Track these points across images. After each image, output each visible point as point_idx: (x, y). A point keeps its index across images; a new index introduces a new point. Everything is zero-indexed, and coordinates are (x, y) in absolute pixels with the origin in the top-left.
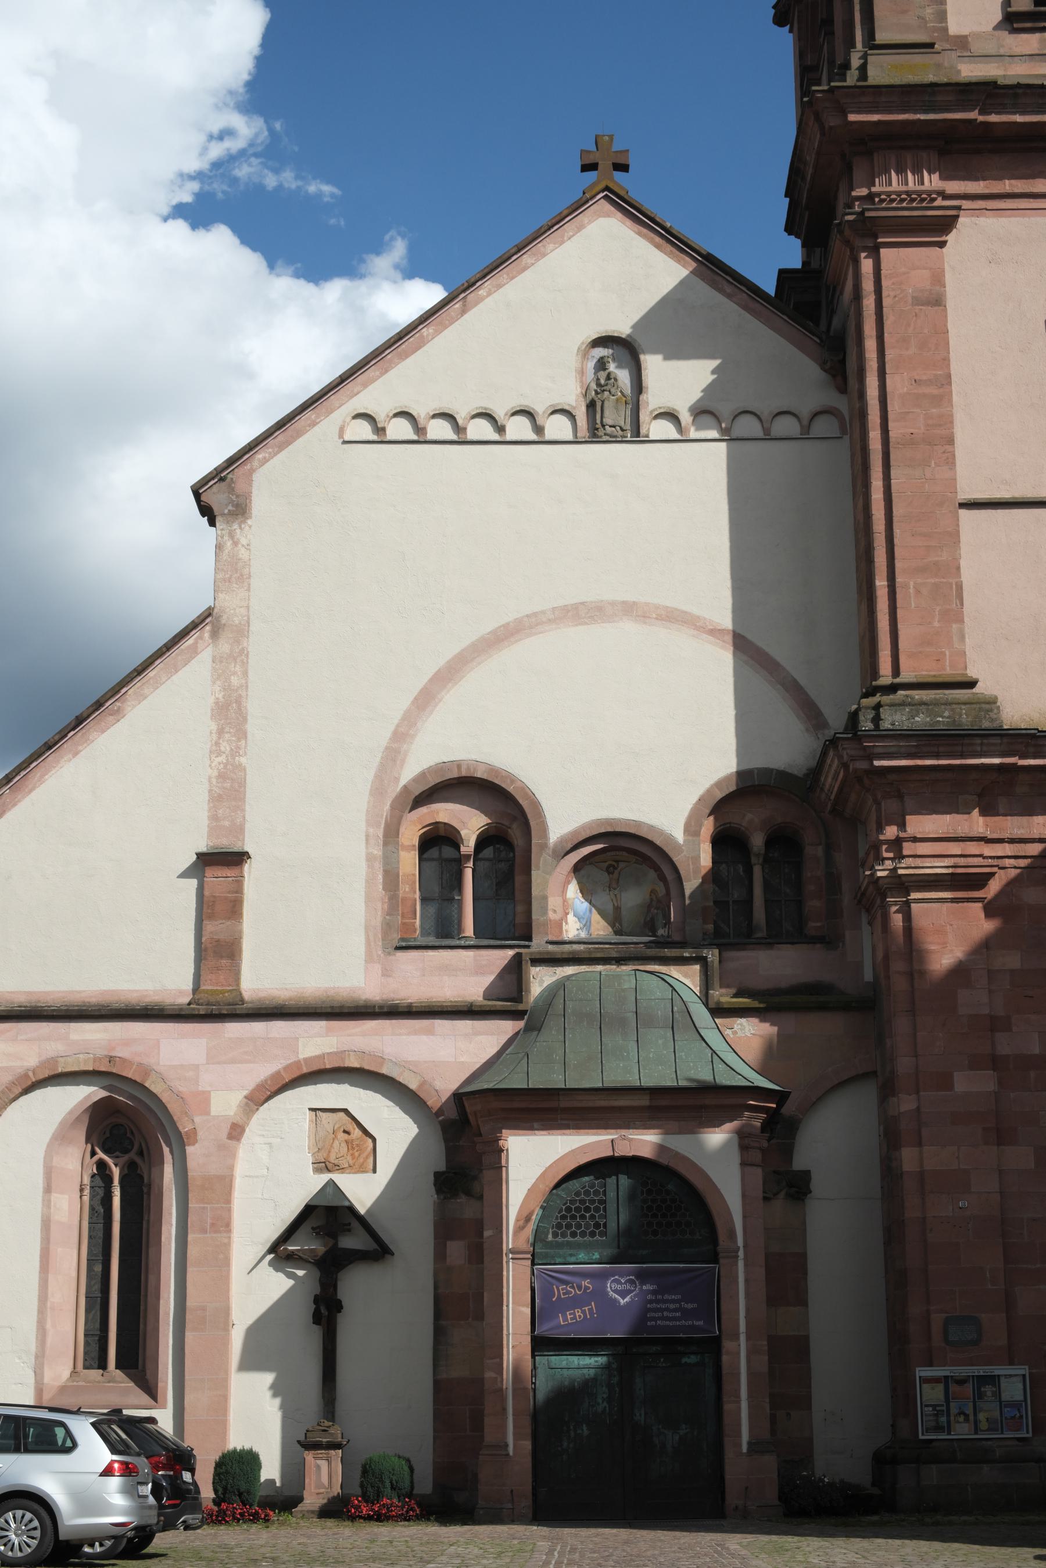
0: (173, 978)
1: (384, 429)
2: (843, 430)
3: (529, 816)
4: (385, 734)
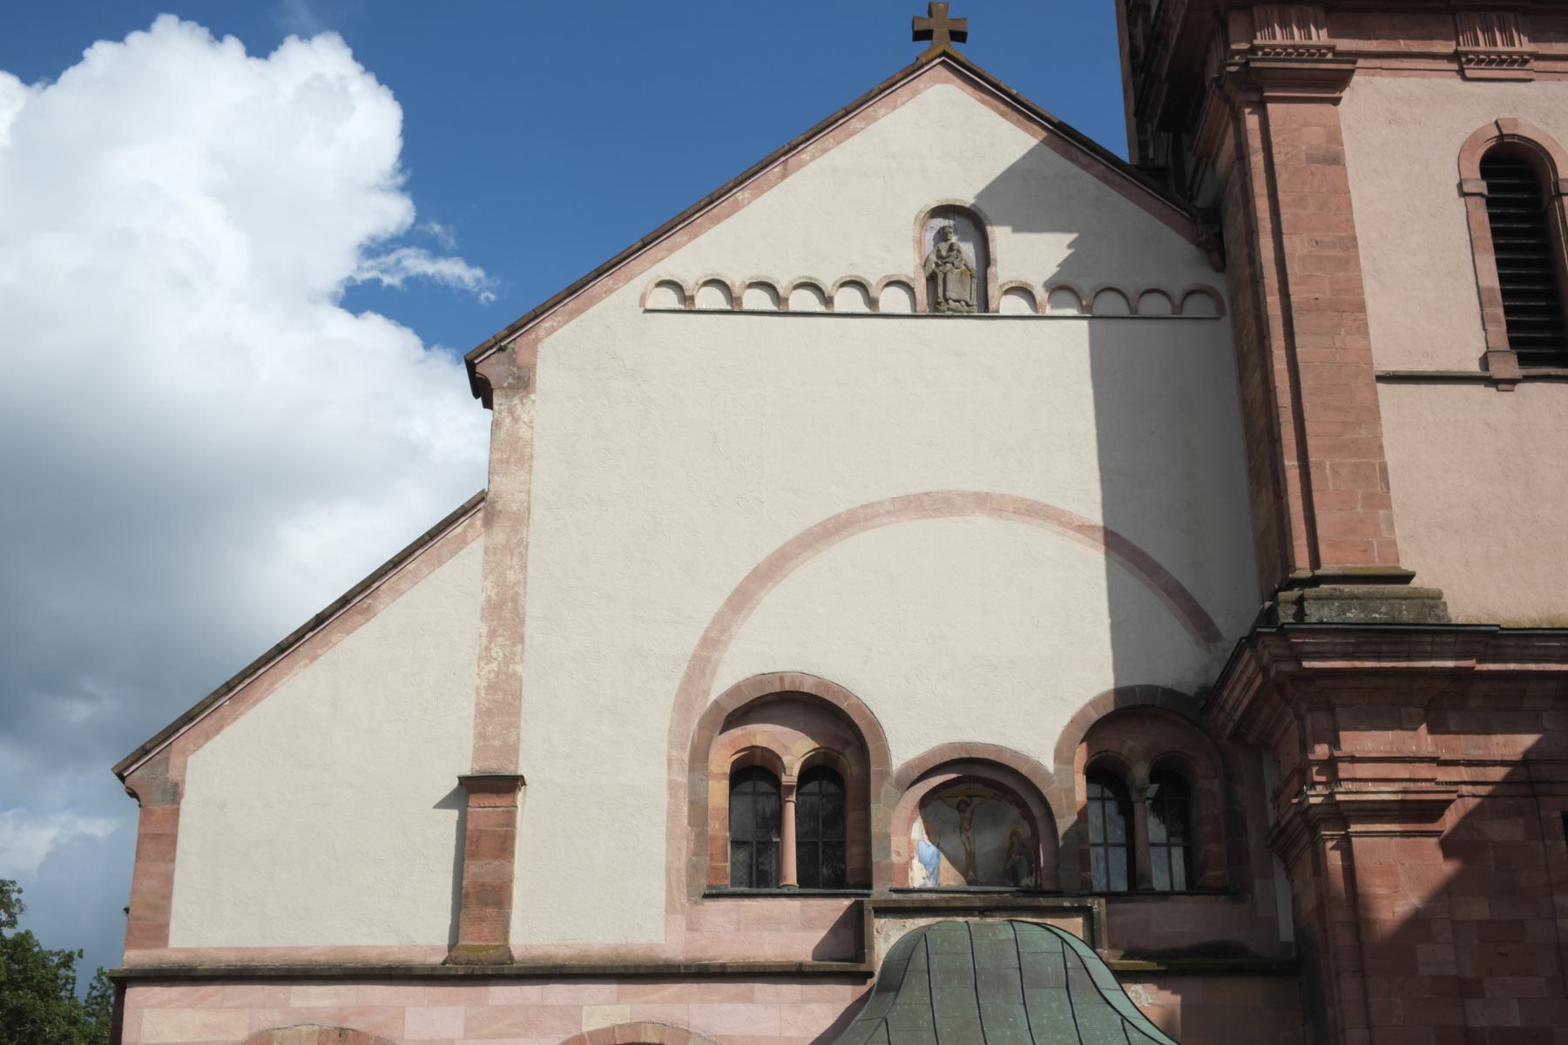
0: (425, 931)
1: (692, 298)
2: (1221, 310)
3: (867, 739)
4: (692, 641)
